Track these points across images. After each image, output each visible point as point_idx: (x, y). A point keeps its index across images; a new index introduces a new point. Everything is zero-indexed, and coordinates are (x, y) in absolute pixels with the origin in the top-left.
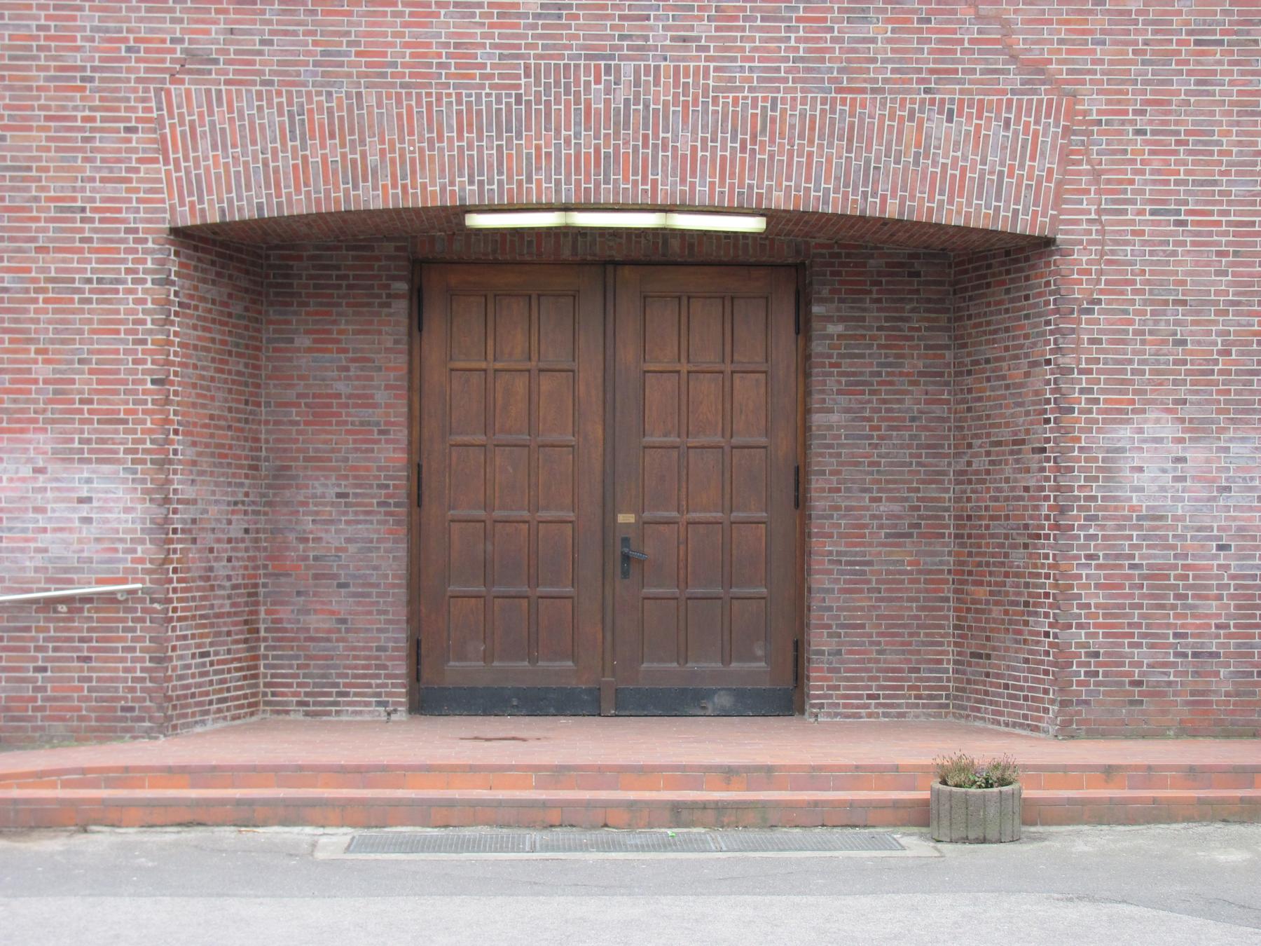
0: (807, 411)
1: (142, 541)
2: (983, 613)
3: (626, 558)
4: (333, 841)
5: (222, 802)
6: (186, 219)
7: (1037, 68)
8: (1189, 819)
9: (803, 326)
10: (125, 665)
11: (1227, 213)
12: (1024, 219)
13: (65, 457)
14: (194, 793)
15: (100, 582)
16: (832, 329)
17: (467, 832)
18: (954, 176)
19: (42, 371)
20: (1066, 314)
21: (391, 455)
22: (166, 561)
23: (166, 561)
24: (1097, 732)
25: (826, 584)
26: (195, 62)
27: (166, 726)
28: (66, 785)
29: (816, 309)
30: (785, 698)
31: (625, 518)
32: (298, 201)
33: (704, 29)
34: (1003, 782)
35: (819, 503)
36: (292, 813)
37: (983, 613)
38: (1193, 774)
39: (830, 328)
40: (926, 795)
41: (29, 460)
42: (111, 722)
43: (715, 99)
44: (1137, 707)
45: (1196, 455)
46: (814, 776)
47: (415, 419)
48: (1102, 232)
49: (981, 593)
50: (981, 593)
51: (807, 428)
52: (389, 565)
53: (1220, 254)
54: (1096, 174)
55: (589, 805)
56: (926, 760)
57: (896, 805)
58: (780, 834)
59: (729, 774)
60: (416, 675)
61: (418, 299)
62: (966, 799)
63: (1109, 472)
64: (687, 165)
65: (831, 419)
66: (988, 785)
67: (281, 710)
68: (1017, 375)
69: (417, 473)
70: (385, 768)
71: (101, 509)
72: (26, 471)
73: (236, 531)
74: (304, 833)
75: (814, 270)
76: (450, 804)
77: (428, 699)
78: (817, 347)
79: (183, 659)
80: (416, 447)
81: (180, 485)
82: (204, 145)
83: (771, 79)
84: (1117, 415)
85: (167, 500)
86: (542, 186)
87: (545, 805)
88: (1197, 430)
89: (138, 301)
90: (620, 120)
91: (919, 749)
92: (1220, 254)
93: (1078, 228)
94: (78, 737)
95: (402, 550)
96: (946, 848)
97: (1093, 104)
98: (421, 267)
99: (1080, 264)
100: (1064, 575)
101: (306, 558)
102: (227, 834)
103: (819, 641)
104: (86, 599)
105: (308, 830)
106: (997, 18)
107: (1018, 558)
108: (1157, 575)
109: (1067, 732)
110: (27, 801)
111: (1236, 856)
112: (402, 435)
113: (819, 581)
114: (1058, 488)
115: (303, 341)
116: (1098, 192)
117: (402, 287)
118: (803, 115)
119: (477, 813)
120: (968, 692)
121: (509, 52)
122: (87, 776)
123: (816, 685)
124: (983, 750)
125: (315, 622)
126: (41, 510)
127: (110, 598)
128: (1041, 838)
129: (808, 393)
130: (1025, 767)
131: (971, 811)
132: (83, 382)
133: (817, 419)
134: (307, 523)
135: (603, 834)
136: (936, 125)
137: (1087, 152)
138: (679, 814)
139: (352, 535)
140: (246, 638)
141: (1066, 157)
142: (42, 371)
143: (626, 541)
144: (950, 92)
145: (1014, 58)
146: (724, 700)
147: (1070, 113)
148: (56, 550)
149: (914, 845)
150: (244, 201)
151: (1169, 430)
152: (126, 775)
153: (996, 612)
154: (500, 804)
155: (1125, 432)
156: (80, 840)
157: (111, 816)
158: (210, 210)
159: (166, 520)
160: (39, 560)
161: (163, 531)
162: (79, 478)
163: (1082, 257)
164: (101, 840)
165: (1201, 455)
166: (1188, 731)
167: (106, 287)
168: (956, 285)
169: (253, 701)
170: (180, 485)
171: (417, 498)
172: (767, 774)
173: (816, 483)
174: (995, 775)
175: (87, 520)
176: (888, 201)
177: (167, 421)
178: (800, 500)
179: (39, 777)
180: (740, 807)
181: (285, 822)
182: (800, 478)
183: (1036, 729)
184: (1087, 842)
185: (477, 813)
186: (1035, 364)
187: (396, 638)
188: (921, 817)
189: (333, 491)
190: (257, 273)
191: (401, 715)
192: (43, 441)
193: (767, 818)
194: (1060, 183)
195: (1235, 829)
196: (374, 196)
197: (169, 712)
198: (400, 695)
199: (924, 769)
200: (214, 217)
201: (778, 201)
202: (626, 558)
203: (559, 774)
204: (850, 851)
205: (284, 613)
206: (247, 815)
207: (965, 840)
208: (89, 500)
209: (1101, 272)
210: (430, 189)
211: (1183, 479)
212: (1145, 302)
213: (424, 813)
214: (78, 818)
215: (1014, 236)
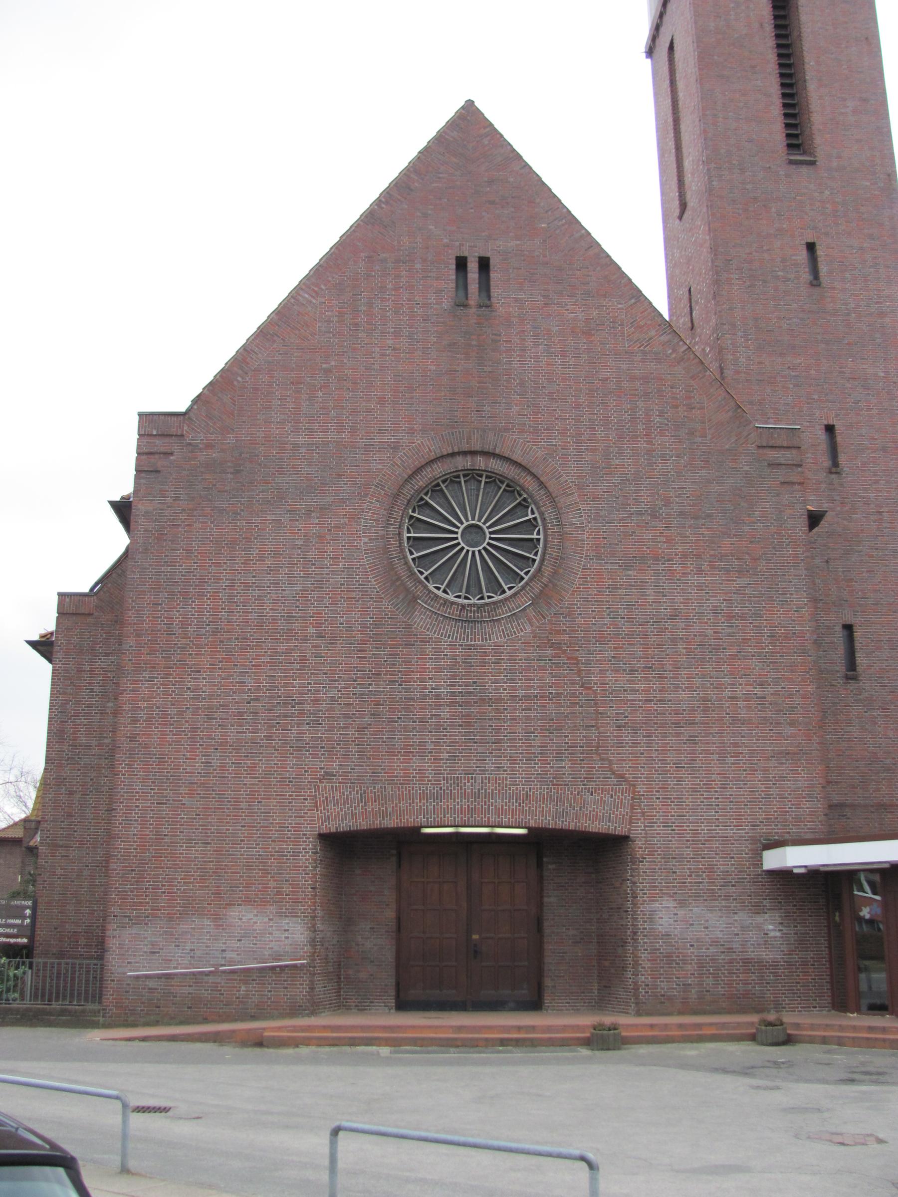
0: (542, 897)
1: (306, 945)
2: (606, 970)
3: (476, 952)
4: (385, 1051)
5: (344, 1038)
6: (324, 830)
7: (622, 776)
8: (679, 1042)
9: (540, 865)
10: (300, 990)
11: (688, 826)
12: (616, 828)
13: (280, 915)
14: (335, 1035)
15: (291, 960)
16: (551, 867)
17: (430, 1048)
18: (595, 815)
19: (272, 884)
20: (634, 863)
21: (390, 914)
22: (315, 952)
23: (315, 952)
24: (649, 1014)
25: (550, 960)
26: (328, 775)
27: (313, 1013)
28: (288, 1031)
29: (545, 859)
30: (535, 1004)
31: (475, 937)
32: (363, 824)
33: (506, 764)
34: (615, 1029)
35: (547, 931)
36: (369, 1042)
37: (606, 970)
38: (681, 1026)
39: (550, 867)
40: (588, 1035)
41: (267, 916)
42: (294, 1011)
43: (510, 789)
44: (662, 1005)
45: (681, 912)
46: (549, 1029)
47: (399, 901)
48: (646, 834)
49: (607, 964)
50: (607, 964)
51: (542, 903)
52: (389, 955)
53: (688, 841)
54: (643, 814)
55: (472, 1039)
56: (589, 1023)
57: (578, 1039)
58: (539, 1048)
59: (519, 1029)
60: (398, 996)
61: (399, 856)
62: (602, 1035)
63: (651, 919)
64: (500, 811)
65: (551, 899)
66: (610, 1030)
67: (348, 1008)
68: (617, 884)
69: (399, 919)
70: (399, 1027)
71: (292, 934)
72: (266, 920)
73: (335, 942)
74: (374, 1048)
75: (545, 847)
76: (423, 1039)
77: (402, 1005)
78: (546, 873)
79: (319, 988)
80: (399, 911)
81: (319, 926)
82: (331, 805)
83: (529, 781)
84: (653, 899)
85: (315, 931)
86: (449, 818)
87: (456, 1039)
88: (682, 903)
89: (307, 860)
90: (476, 796)
91: (587, 1020)
92: (688, 841)
93: (637, 831)
94: (282, 1016)
95: (394, 950)
96: (596, 1052)
97: (641, 789)
98: (400, 846)
99: (639, 845)
100: (636, 957)
101: (358, 952)
102: (347, 1049)
103: (548, 982)
104: (286, 966)
105: (374, 1048)
106: (607, 759)
107: (620, 951)
108: (669, 956)
109: (638, 1014)
110: (278, 1037)
111: (693, 1053)
112: (394, 906)
113: (547, 960)
114: (633, 925)
115: (358, 871)
116: (645, 819)
117: (394, 852)
118: (540, 793)
119: (433, 1042)
120: (601, 1003)
121: (438, 773)
122: (295, 1029)
123: (547, 1000)
124: (608, 1020)
125: (363, 975)
126: (271, 934)
127: (295, 966)
128: (628, 1049)
129: (542, 890)
130: (623, 1025)
131: (604, 1041)
132: (287, 888)
133: (546, 900)
134: (359, 938)
135: (477, 1049)
136: (588, 797)
137: (640, 806)
138: (503, 1042)
139: (376, 944)
140: (338, 980)
141: (632, 808)
142: (272, 884)
143: (475, 945)
144: (592, 785)
145: (614, 773)
146: (512, 1005)
147: (634, 792)
148: (276, 948)
149: (585, 1052)
150: (344, 825)
151: (672, 904)
152: (309, 1028)
153: (612, 971)
154: (440, 1039)
155: (657, 905)
156: (297, 1050)
157: (307, 1042)
158: (333, 826)
159: (315, 938)
160: (270, 952)
161: (313, 942)
162: (285, 922)
163: (639, 843)
164: (304, 1050)
165: (683, 912)
166: (681, 1013)
167: (295, 854)
168: (596, 854)
169: (341, 1005)
170: (319, 926)
171: (399, 929)
172: (533, 1028)
173: (546, 924)
174: (612, 1027)
175: (287, 938)
176: (570, 824)
177: (316, 902)
178: (540, 929)
179: (279, 1029)
180: (524, 1039)
181: (366, 1045)
182: (539, 922)
183: (627, 1013)
184: (643, 1050)
185: (433, 1042)
186: (624, 880)
187: (392, 981)
188: (587, 1043)
189: (368, 927)
190: (345, 849)
191: (393, 1011)
192: (272, 909)
193: (533, 1044)
194: (631, 817)
195: (695, 1045)
196: (390, 823)
197: (314, 1008)
198: (392, 1003)
199: (587, 1026)
200: (334, 830)
201: (532, 824)
202: (476, 952)
203: (460, 1029)
204: (228, 1050)
205: (351, 972)
206: (353, 1042)
207: (602, 1049)
208: (288, 930)
209: (646, 848)
210: (409, 821)
211: (676, 921)
212: (662, 858)
213: (414, 1042)
214: (295, 1043)
215: (615, 835)
